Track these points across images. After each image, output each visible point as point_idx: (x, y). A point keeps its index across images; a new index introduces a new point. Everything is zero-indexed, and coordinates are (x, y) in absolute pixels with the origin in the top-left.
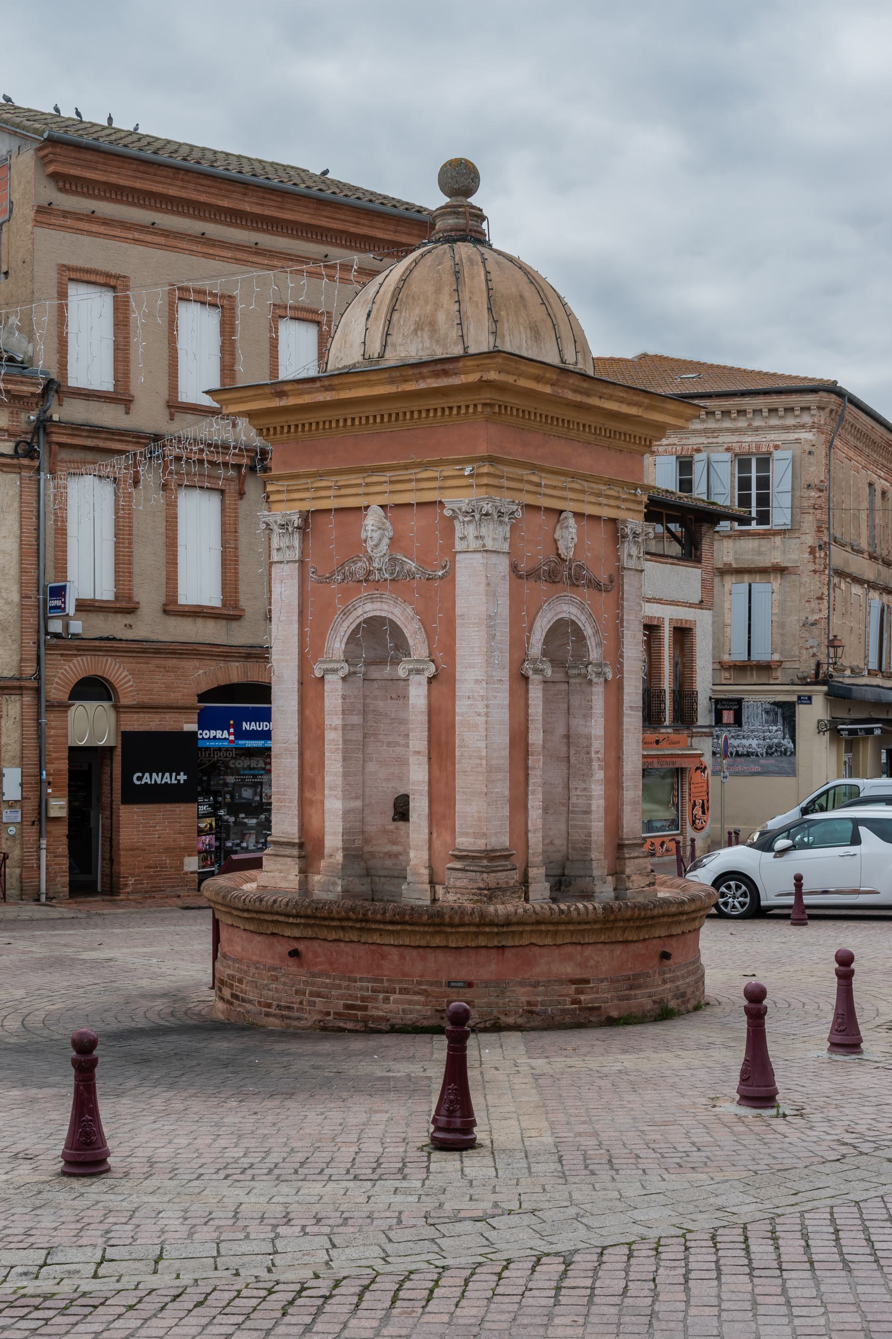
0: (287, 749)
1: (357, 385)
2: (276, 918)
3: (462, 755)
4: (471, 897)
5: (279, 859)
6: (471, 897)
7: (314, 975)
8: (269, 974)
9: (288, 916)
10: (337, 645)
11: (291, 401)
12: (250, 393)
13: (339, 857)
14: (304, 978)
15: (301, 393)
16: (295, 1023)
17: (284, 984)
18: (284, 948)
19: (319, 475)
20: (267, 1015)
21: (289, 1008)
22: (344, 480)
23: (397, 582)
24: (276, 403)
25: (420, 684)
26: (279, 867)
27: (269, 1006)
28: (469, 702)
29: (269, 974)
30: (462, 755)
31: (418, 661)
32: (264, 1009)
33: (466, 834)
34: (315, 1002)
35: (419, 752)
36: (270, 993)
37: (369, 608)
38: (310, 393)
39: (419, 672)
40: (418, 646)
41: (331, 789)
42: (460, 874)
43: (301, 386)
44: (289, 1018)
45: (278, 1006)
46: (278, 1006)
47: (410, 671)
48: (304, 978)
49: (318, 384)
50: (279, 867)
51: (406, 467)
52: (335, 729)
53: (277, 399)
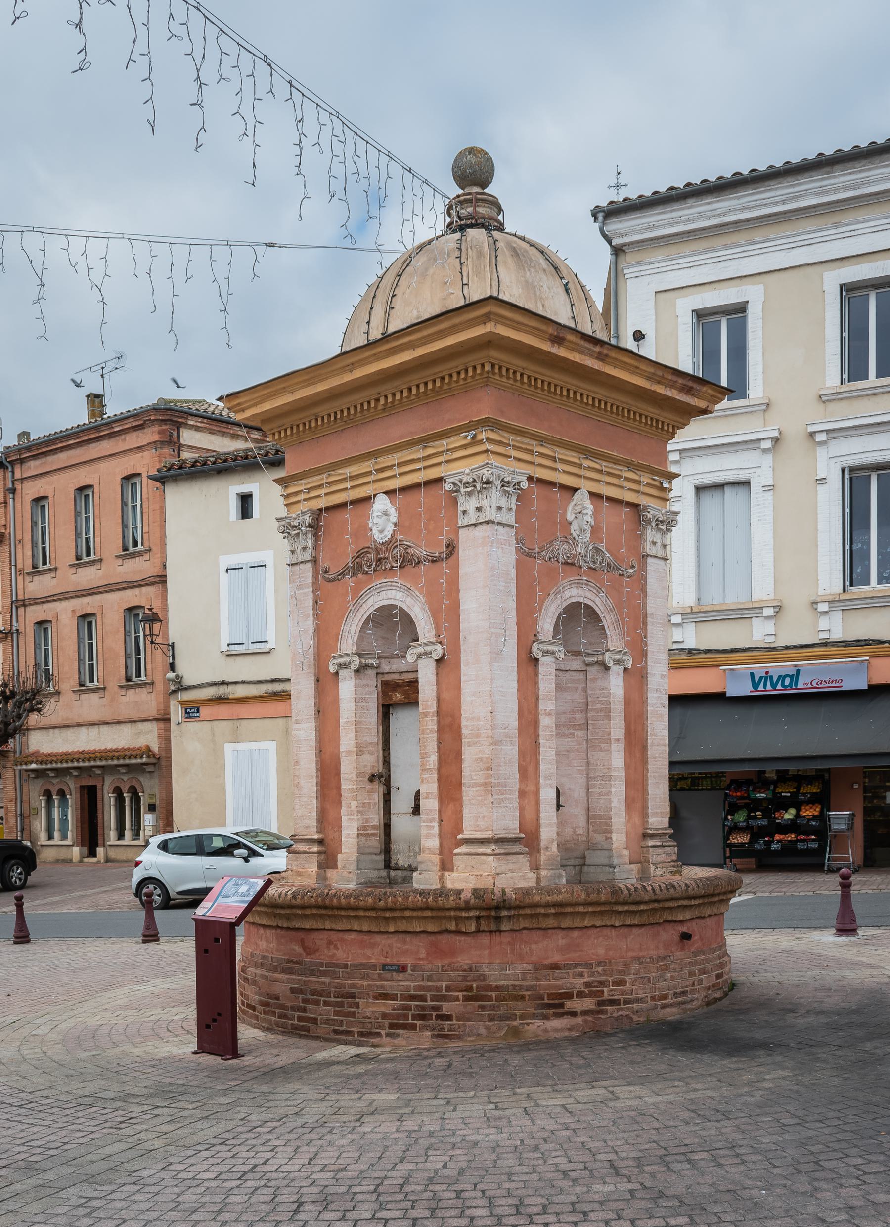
0: (507, 735)
1: (625, 367)
2: (681, 903)
3: (653, 743)
4: (672, 869)
5: (510, 857)
6: (672, 869)
7: (696, 954)
8: (657, 965)
9: (690, 898)
10: (546, 625)
11: (562, 352)
12: (534, 323)
13: (554, 848)
14: (689, 960)
15: (574, 348)
16: (689, 1006)
17: (674, 970)
18: (671, 934)
19: (542, 440)
20: (664, 1007)
21: (684, 993)
22: (561, 453)
23: (593, 571)
24: (546, 346)
25: (618, 674)
26: (511, 866)
27: (665, 997)
28: (657, 695)
29: (657, 965)
30: (653, 743)
31: (426, 644)
32: (659, 1003)
33: (655, 814)
34: (701, 980)
35: (618, 740)
36: (666, 983)
37: (573, 594)
38: (581, 352)
39: (427, 654)
40: (425, 629)
41: (546, 778)
42: (659, 850)
43: (582, 342)
44: (684, 1003)
45: (675, 994)
46: (675, 994)
47: (420, 655)
48: (689, 960)
49: (597, 349)
50: (511, 866)
51: (616, 462)
52: (550, 714)
53: (549, 343)
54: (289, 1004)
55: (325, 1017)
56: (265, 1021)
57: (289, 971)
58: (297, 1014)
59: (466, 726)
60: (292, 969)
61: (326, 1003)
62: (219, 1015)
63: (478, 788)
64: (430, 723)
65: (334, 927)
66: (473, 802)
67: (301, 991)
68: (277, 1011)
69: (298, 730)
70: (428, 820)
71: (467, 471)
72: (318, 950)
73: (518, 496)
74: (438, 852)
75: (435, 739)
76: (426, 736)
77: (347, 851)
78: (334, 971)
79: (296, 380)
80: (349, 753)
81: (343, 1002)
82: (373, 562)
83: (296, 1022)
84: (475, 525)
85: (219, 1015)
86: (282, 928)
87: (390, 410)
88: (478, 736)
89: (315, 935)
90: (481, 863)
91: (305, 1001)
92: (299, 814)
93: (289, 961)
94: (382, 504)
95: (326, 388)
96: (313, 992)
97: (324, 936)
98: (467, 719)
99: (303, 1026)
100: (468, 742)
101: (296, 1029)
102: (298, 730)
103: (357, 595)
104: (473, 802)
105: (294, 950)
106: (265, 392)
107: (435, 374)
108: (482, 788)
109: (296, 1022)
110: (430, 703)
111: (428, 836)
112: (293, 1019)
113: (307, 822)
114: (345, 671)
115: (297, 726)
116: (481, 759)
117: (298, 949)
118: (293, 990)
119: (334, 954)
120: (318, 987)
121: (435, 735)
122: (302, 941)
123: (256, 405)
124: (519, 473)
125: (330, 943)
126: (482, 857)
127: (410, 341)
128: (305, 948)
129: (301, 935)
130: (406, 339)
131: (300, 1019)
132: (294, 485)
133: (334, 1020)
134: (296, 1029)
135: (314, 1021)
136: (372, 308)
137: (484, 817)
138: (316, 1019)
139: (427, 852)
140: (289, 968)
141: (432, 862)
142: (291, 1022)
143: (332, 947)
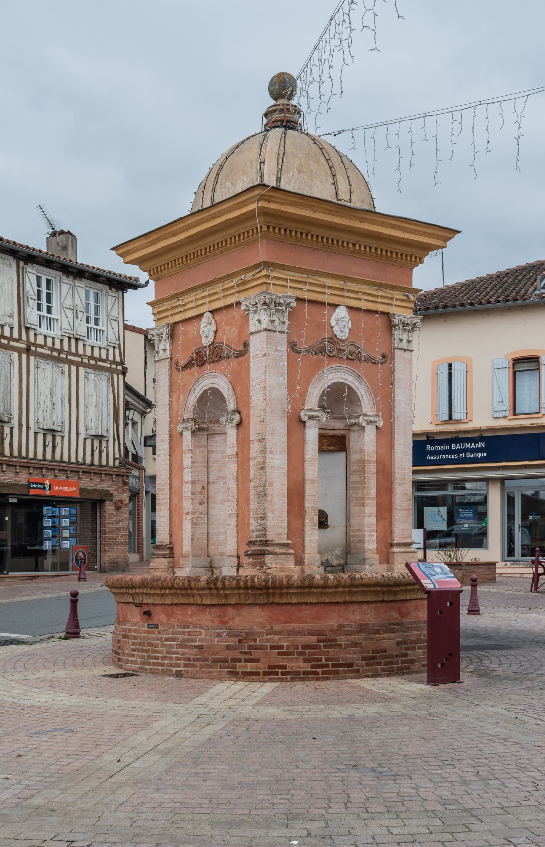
54: (395, 654)
55: (418, 657)
56: (369, 671)
57: (392, 631)
58: (400, 660)
59: (398, 472)
60: (394, 629)
61: (419, 648)
62: (451, 654)
63: (404, 512)
64: (372, 467)
65: (395, 599)
66: (401, 520)
67: (404, 643)
68: (383, 661)
69: (272, 459)
70: (370, 531)
71: (408, 317)
72: (409, 614)
73: (289, 312)
74: (376, 552)
75: (375, 478)
76: (369, 475)
77: (309, 552)
78: (420, 626)
79: (325, 207)
80: (313, 481)
81: (278, 672)
82: (330, 349)
83: (400, 665)
84: (405, 350)
85: (451, 654)
86: (388, 602)
87: (355, 253)
88: (404, 479)
89: (408, 604)
90: (411, 558)
91: (407, 649)
92: (272, 525)
93: (390, 624)
94: (341, 312)
95: (342, 223)
96: (413, 642)
97: (413, 603)
98: (399, 468)
99: (405, 667)
100: (399, 483)
101: (400, 669)
102: (272, 459)
103: (317, 367)
104: (401, 520)
105: (392, 616)
106: (299, 201)
107: (395, 249)
108: (406, 512)
109: (400, 665)
110: (372, 455)
111: (370, 541)
112: (398, 663)
113: (278, 530)
114: (312, 421)
115: (271, 456)
116: (406, 494)
117: (395, 615)
118: (398, 643)
119: (418, 615)
120: (414, 638)
121: (375, 475)
122: (399, 609)
123: (282, 204)
124: (287, 295)
125: (416, 608)
126: (412, 554)
127: (408, 228)
128: (400, 613)
129: (398, 605)
130: (406, 225)
131: (403, 662)
132: (278, 272)
133: (423, 658)
134: (400, 669)
135: (413, 661)
136: (348, 177)
137: (407, 529)
138: (413, 660)
139: (369, 552)
140: (391, 629)
141: (375, 558)
142: (395, 666)
143: (417, 610)
